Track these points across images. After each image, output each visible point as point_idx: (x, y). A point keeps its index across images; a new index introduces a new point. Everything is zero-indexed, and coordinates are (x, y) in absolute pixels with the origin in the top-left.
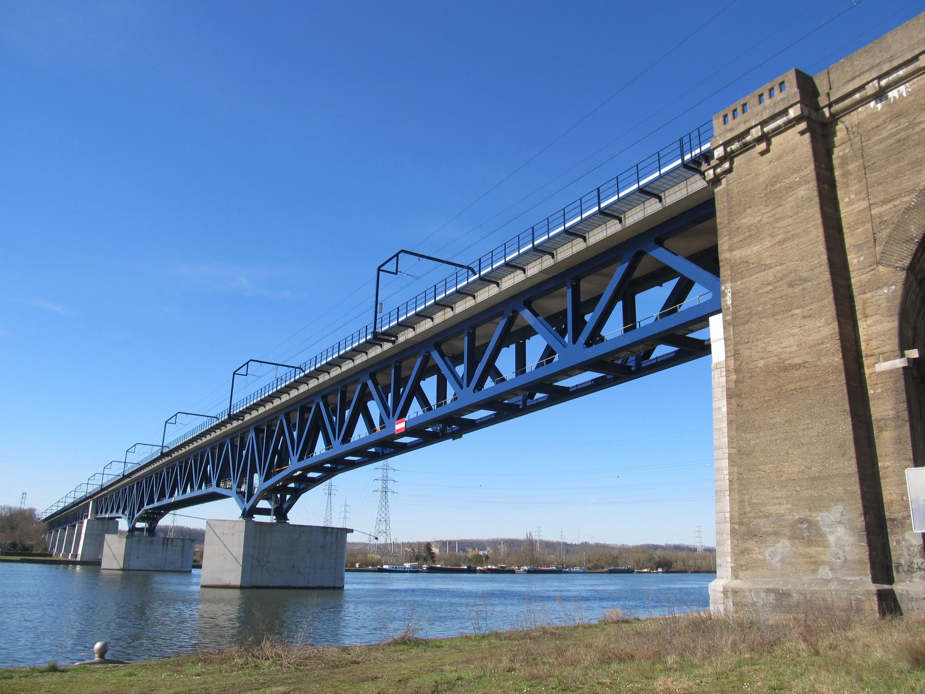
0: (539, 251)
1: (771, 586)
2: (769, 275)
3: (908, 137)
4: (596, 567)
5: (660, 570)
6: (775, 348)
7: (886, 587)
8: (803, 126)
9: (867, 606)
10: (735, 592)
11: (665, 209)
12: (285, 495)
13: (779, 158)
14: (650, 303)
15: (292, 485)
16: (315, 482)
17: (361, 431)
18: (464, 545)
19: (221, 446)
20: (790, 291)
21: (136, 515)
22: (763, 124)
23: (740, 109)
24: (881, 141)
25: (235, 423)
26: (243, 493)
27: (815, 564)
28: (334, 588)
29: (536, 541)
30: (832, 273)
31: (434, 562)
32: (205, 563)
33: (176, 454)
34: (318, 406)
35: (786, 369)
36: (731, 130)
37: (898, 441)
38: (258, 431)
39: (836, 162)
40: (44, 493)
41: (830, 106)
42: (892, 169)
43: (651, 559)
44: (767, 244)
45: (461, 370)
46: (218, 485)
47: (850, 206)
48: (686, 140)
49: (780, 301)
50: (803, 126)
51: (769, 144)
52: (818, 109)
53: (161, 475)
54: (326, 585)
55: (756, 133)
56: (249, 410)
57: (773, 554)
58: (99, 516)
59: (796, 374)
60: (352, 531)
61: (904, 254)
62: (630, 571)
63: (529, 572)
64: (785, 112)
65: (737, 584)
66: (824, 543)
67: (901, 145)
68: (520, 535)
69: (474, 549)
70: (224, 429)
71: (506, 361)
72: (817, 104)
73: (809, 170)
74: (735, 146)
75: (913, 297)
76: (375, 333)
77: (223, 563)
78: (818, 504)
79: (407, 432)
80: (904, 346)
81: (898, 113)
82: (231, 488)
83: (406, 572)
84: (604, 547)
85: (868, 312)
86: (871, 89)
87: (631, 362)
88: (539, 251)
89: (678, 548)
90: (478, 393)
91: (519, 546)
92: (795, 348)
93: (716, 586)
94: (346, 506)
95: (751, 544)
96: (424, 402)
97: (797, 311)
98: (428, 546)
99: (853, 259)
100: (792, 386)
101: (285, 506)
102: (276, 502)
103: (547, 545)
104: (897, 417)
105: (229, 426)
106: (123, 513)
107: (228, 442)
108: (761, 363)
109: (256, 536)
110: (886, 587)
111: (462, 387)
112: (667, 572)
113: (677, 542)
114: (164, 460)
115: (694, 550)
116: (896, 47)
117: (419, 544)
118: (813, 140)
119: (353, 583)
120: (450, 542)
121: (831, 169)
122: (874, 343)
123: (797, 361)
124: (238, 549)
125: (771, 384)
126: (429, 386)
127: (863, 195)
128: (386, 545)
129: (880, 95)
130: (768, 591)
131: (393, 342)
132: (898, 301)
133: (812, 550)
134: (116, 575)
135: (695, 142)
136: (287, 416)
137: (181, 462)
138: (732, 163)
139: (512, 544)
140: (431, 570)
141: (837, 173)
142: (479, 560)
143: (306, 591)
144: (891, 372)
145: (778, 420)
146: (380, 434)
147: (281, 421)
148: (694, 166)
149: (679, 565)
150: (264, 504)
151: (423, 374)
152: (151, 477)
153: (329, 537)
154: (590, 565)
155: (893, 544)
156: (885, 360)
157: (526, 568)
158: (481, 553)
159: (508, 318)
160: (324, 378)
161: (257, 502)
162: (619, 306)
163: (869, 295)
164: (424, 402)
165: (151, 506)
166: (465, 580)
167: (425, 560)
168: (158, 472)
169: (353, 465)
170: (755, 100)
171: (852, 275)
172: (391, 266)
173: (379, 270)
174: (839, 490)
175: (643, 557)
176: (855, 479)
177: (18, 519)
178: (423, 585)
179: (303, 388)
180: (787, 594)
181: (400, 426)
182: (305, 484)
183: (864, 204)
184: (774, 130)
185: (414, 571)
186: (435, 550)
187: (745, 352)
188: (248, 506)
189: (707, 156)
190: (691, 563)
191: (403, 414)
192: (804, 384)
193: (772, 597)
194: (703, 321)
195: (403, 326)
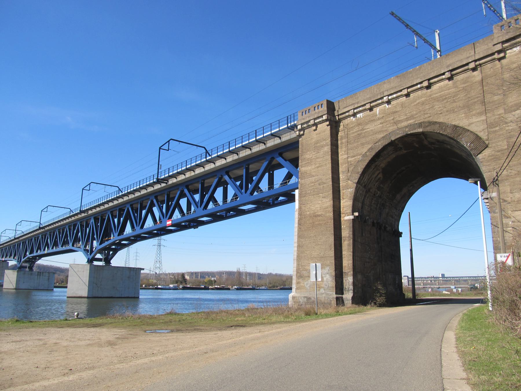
0: (231, 152)
1: (306, 295)
2: (313, 179)
3: (361, 134)
4: (274, 287)
6: (313, 208)
7: (340, 296)
8: (328, 123)
9: (333, 302)
11: (282, 143)
12: (109, 252)
13: (319, 134)
14: (279, 175)
15: (114, 247)
16: (125, 246)
17: (149, 223)
18: (203, 275)
19: (75, 226)
20: (319, 186)
21: (23, 260)
22: (315, 119)
23: (307, 111)
24: (353, 133)
25: (83, 215)
26: (88, 251)
28: (134, 298)
29: (243, 273)
30: (332, 182)
31: (186, 284)
32: (69, 285)
33: (48, 228)
34: (128, 209)
35: (316, 216)
36: (304, 119)
37: (349, 245)
38: (96, 219)
39: (339, 138)
41: (338, 116)
42: (355, 144)
44: (313, 167)
45: (197, 197)
46: (73, 245)
47: (342, 157)
48: (289, 117)
49: (316, 190)
50: (328, 123)
51: (317, 127)
52: (334, 116)
53: (38, 238)
54: (130, 296)
55: (312, 122)
56: (91, 209)
57: (307, 284)
59: (319, 218)
60: (143, 269)
61: (356, 177)
63: (237, 289)
64: (322, 116)
68: (232, 268)
69: (209, 277)
70: (76, 217)
71: (219, 195)
72: (334, 114)
73: (329, 141)
74: (305, 125)
75: (361, 192)
76: (158, 179)
77: (79, 285)
79: (172, 225)
80: (353, 211)
82: (79, 247)
83: (171, 289)
84: (281, 276)
85: (344, 197)
86: (351, 113)
87: (271, 201)
88: (231, 152)
90: (205, 211)
92: (319, 209)
93: (291, 295)
94: (137, 253)
95: (300, 280)
96: (181, 211)
97: (321, 195)
98: (183, 275)
99: (341, 176)
100: (317, 223)
101: (110, 257)
102: (105, 255)
103: (251, 274)
104: (349, 237)
105: (80, 216)
106: (14, 258)
107: (79, 223)
108: (308, 213)
109: (94, 272)
110: (340, 296)
111: (198, 207)
114: (40, 231)
117: (178, 274)
119: (144, 295)
120: (196, 273)
121: (337, 140)
122: (345, 209)
123: (319, 213)
124: (86, 279)
125: (311, 221)
126: (183, 202)
127: (346, 153)
128: (160, 274)
129: (354, 115)
130: (305, 297)
131: (166, 183)
132: (353, 195)
135: (292, 119)
136: (112, 212)
137: (51, 232)
138: (304, 132)
139: (230, 274)
140: (184, 288)
141: (339, 142)
142: (211, 282)
143: (133, 299)
144: (349, 220)
145: (312, 235)
146: (159, 226)
147: (109, 216)
148: (293, 128)
150: (99, 256)
151: (182, 195)
152: (31, 240)
153: (132, 272)
154: (270, 286)
155: (344, 281)
156: (348, 216)
157: (236, 287)
158: (213, 279)
159: (221, 177)
160: (131, 196)
161: (95, 255)
162: (267, 175)
163: (344, 191)
164: (181, 211)
165: (32, 255)
166: (202, 293)
167: (181, 283)
168: (36, 237)
169: (145, 238)
170: (313, 109)
171: (341, 182)
172: (165, 147)
173: (160, 148)
174: (328, 262)
176: (333, 258)
178: (181, 296)
179: (121, 200)
180: (310, 298)
181: (169, 223)
182: (120, 246)
183: (346, 156)
184: (319, 122)
185: (175, 289)
186: (187, 277)
187: (303, 208)
188: (91, 257)
189: (295, 126)
191: (171, 217)
192: (321, 222)
193: (306, 299)
194: (294, 190)
195: (171, 177)
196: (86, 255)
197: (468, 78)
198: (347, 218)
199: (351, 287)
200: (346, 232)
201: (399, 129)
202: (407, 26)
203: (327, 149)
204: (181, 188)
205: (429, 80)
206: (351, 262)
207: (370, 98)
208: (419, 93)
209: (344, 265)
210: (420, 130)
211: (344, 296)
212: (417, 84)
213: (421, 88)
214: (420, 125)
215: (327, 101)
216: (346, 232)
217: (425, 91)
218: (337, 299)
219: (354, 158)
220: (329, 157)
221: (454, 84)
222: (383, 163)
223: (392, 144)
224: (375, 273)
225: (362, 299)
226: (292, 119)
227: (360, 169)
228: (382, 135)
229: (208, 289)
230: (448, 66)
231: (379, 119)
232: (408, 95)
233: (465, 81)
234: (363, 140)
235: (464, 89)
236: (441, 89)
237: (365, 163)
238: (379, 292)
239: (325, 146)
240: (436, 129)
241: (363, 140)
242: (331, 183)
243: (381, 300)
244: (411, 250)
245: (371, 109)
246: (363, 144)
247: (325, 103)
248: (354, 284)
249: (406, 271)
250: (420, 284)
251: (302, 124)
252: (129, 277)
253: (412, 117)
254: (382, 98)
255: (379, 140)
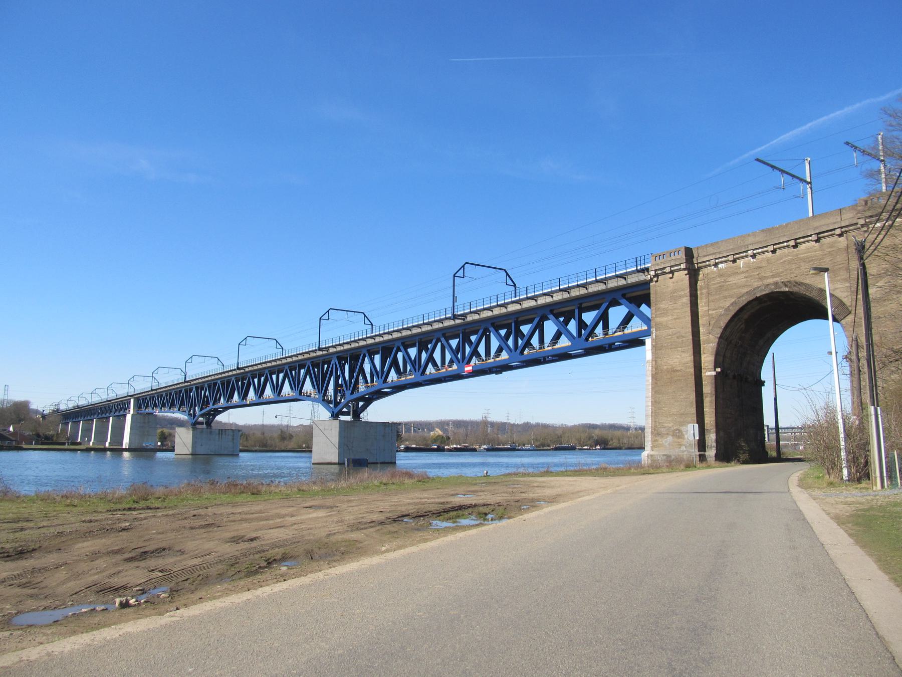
5: (598, 447)
8: (686, 272)
10: (652, 456)
27: (680, 445)
37: (711, 402)
40: (48, 391)
43: (590, 438)
44: (670, 318)
47: (702, 308)
50: (686, 272)
52: (693, 264)
55: (668, 270)
58: (143, 411)
61: (718, 332)
62: (573, 448)
63: (488, 450)
64: (680, 265)
65: (652, 453)
66: (684, 438)
67: (721, 288)
77: (327, 447)
78: (684, 423)
80: (715, 367)
81: (721, 275)
84: (545, 426)
89: (613, 427)
91: (448, 425)
93: (645, 454)
99: (702, 330)
112: (604, 449)
113: (612, 422)
115: (628, 429)
116: (722, 248)
118: (690, 278)
121: (696, 290)
124: (336, 440)
125: (669, 376)
129: (716, 265)
133: (680, 440)
134: (184, 459)
135: (643, 262)
149: (615, 443)
154: (538, 443)
157: (485, 447)
173: (454, 276)
175: (583, 436)
177: (20, 411)
180: (670, 456)
183: (707, 308)
187: (659, 360)
188: (336, 411)
190: (625, 441)
191: (468, 362)
196: (328, 409)
197: (834, 242)
198: (709, 373)
199: (714, 444)
200: (708, 389)
201: (765, 285)
202: (773, 167)
203: (686, 300)
204: (484, 326)
205: (796, 239)
206: (714, 419)
207: (733, 250)
208: (786, 250)
209: (706, 422)
210: (787, 289)
211: (707, 453)
212: (783, 242)
213: (788, 246)
214: (786, 283)
215: (686, 248)
216: (708, 389)
217: (791, 250)
218: (700, 456)
219: (716, 312)
220: (688, 309)
221: (821, 246)
222: (745, 316)
223: (757, 299)
224: (739, 428)
225: (725, 455)
226: (643, 262)
227: (723, 324)
228: (745, 290)
229: (443, 450)
230: (815, 228)
231: (743, 272)
232: (774, 251)
233: (831, 245)
234: (726, 293)
235: (830, 253)
236: (808, 250)
237: (729, 318)
238: (742, 449)
239: (683, 296)
240: (802, 290)
241: (726, 293)
242: (691, 337)
243: (743, 457)
244: (775, 399)
245: (734, 261)
246: (725, 297)
247: (683, 250)
248: (717, 441)
249: (768, 420)
250: (788, 439)
251: (655, 271)
252: (384, 436)
253: (778, 275)
254: (746, 251)
255: (743, 295)
